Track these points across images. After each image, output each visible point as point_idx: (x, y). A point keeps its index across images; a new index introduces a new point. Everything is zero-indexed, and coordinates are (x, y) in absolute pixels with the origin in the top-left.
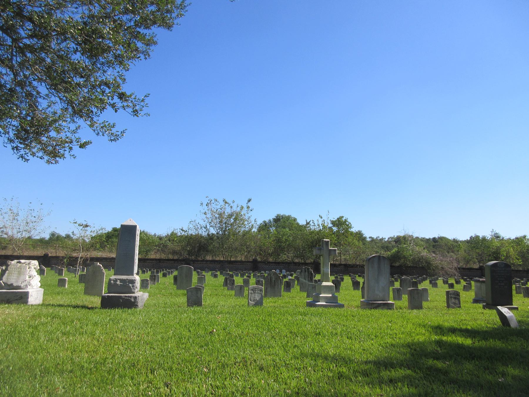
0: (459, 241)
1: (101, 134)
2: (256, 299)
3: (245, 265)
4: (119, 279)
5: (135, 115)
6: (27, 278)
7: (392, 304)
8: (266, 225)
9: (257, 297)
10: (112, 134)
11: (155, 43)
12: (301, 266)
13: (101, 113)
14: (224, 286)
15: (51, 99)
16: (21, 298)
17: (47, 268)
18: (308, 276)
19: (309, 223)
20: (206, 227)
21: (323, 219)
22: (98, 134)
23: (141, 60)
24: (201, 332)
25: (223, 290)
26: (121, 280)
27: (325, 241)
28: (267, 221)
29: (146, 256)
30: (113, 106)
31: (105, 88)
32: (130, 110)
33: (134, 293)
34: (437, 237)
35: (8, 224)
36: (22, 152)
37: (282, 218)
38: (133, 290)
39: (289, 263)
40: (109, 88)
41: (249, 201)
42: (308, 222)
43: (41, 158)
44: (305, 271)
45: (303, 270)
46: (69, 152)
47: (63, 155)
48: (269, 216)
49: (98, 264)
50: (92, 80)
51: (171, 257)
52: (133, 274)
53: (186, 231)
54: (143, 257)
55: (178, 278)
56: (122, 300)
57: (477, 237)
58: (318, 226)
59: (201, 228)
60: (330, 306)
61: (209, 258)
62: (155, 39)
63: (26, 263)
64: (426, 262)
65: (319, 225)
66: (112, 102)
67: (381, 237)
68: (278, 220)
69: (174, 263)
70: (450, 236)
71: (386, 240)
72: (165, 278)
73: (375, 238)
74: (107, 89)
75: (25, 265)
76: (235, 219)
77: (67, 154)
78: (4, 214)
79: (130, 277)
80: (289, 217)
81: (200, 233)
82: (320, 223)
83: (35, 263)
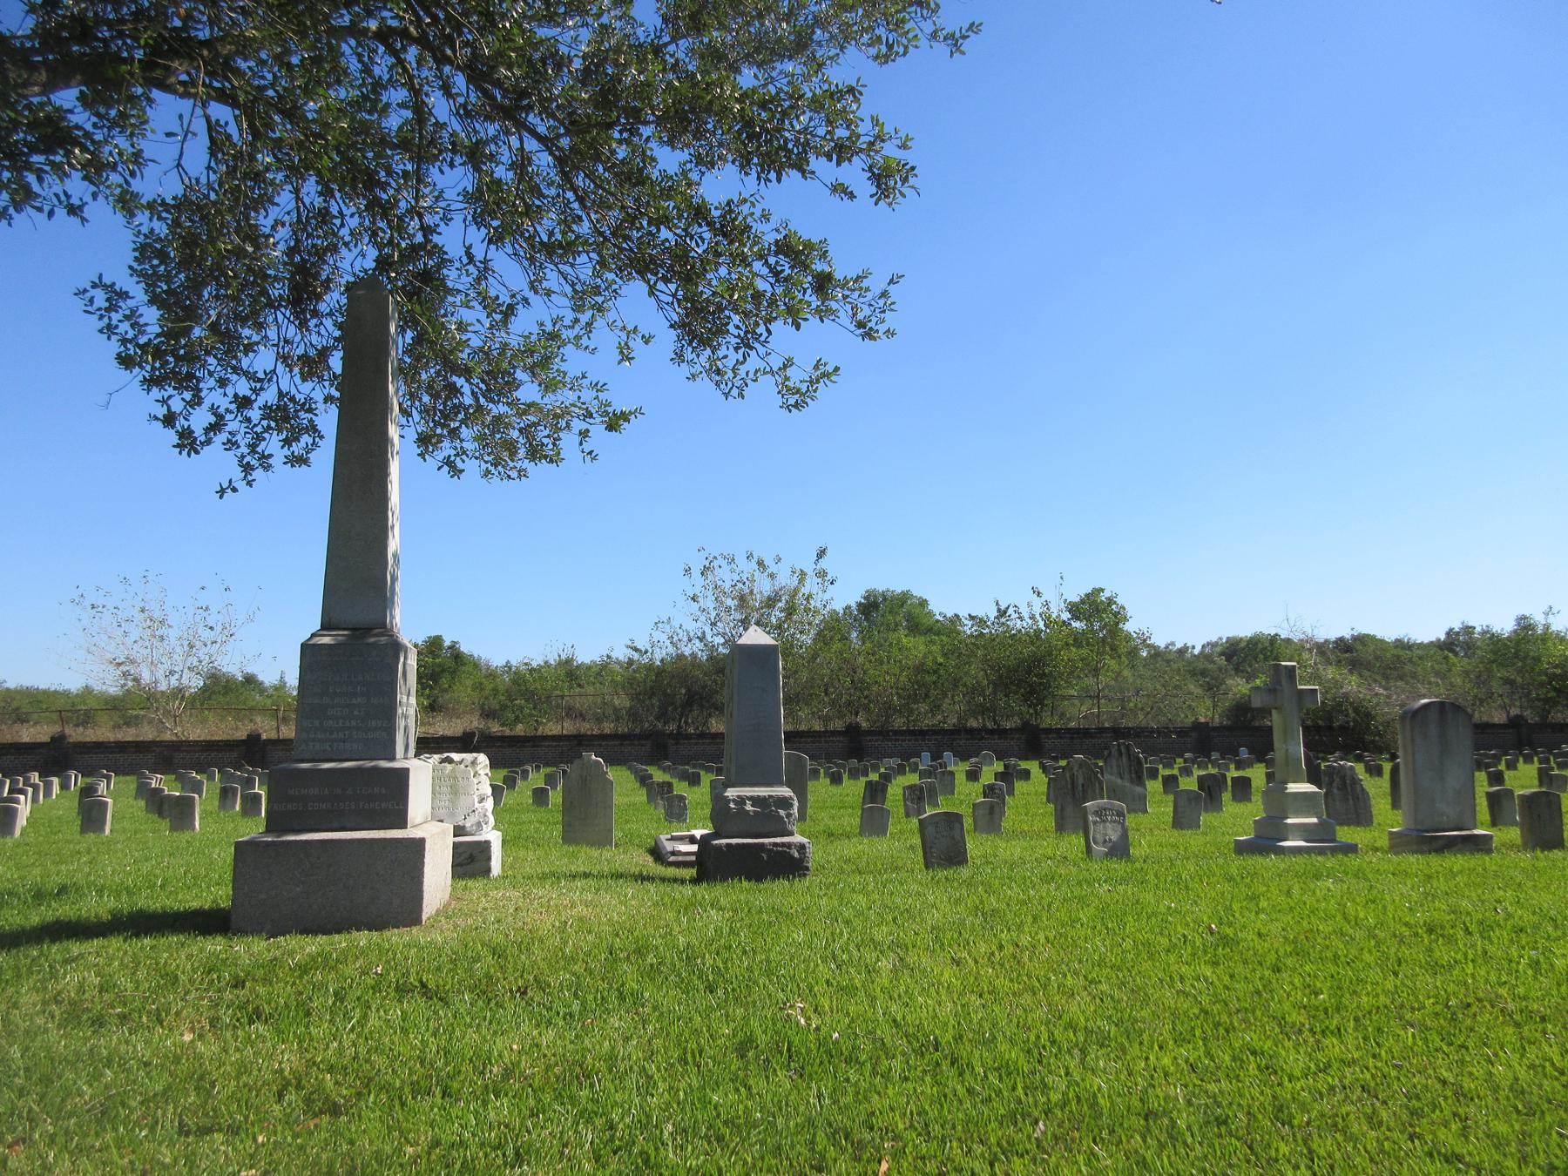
0: (1415, 644)
4: (751, 798)
7: (1488, 838)
8: (838, 620)
17: (122, 778)
19: (1005, 612)
21: (1043, 599)
26: (756, 801)
27: (1286, 666)
29: (536, 729)
33: (791, 834)
34: (1348, 636)
35: (139, 653)
37: (885, 599)
38: (790, 827)
39: (954, 732)
41: (821, 554)
42: (1003, 608)
44: (1120, 754)
45: (1114, 751)
46: (581, 444)
53: (646, 652)
57: (1468, 630)
58: (1030, 622)
59: (690, 640)
60: (1321, 851)
63: (465, 762)
64: (1356, 711)
65: (1032, 617)
67: (1179, 645)
68: (871, 606)
69: (621, 745)
70: (1387, 631)
71: (1196, 652)
73: (1163, 646)
75: (462, 766)
76: (790, 610)
80: (905, 597)
82: (1037, 610)
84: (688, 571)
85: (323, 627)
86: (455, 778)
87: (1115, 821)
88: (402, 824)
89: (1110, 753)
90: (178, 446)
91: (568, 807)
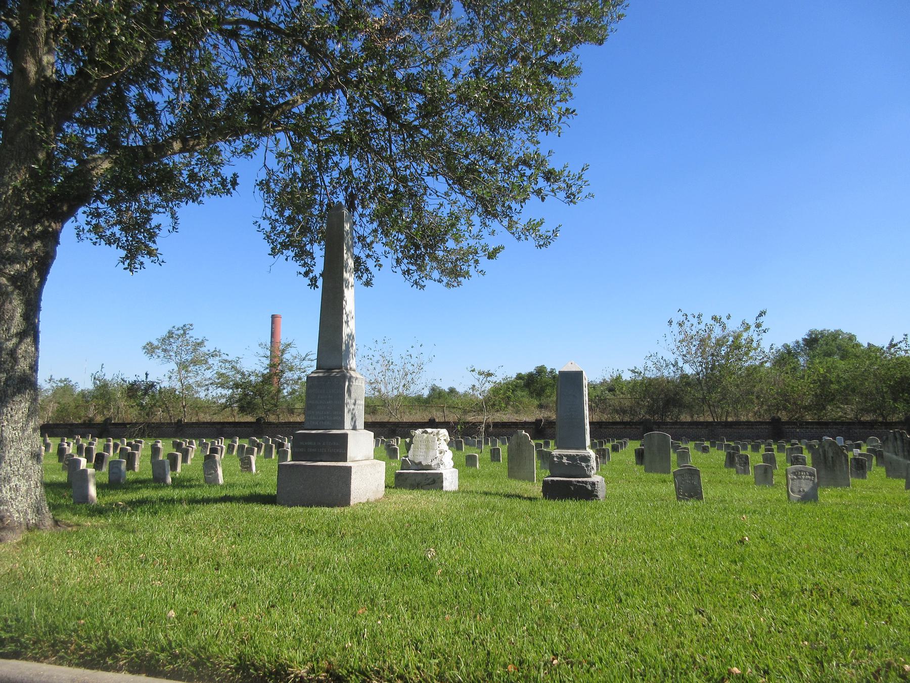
1: (523, 237)
2: (804, 490)
3: (757, 428)
5: (571, 201)
6: (438, 455)
8: (789, 352)
9: (806, 486)
10: (540, 236)
11: (578, 71)
12: (875, 429)
13: (522, 207)
14: (726, 466)
15: (451, 198)
16: (434, 482)
18: (903, 447)
20: (675, 364)
22: (519, 238)
23: (576, 115)
24: (725, 540)
25: (729, 473)
26: (569, 457)
28: (791, 345)
30: (538, 192)
31: (524, 168)
32: (562, 195)
33: (589, 476)
36: (416, 276)
38: (588, 473)
39: (850, 424)
40: (530, 167)
43: (440, 281)
44: (896, 439)
47: (467, 273)
48: (793, 333)
49: (524, 432)
50: (505, 159)
51: (617, 418)
52: (585, 449)
54: (596, 418)
55: (646, 454)
56: (574, 488)
61: (685, 418)
62: (577, 64)
66: (536, 188)
68: (812, 341)
72: (615, 454)
74: (527, 169)
77: (472, 270)
78: (374, 363)
79: (581, 452)
81: (666, 374)
83: (444, 432)
84: (670, 322)
85: (317, 369)
86: (428, 441)
87: (808, 479)
88: (345, 460)
89: (887, 439)
90: (309, 285)
91: (511, 458)
